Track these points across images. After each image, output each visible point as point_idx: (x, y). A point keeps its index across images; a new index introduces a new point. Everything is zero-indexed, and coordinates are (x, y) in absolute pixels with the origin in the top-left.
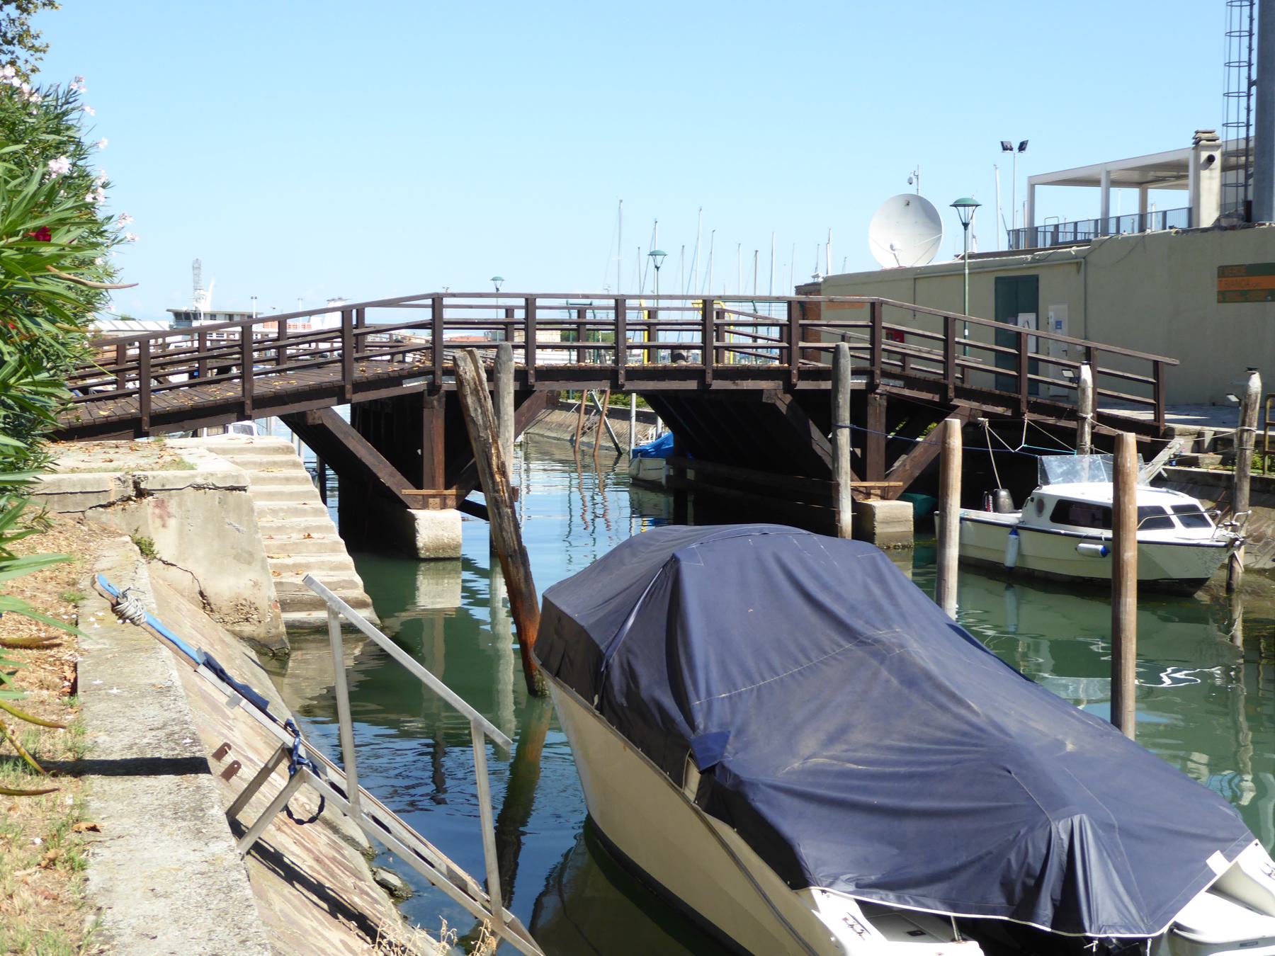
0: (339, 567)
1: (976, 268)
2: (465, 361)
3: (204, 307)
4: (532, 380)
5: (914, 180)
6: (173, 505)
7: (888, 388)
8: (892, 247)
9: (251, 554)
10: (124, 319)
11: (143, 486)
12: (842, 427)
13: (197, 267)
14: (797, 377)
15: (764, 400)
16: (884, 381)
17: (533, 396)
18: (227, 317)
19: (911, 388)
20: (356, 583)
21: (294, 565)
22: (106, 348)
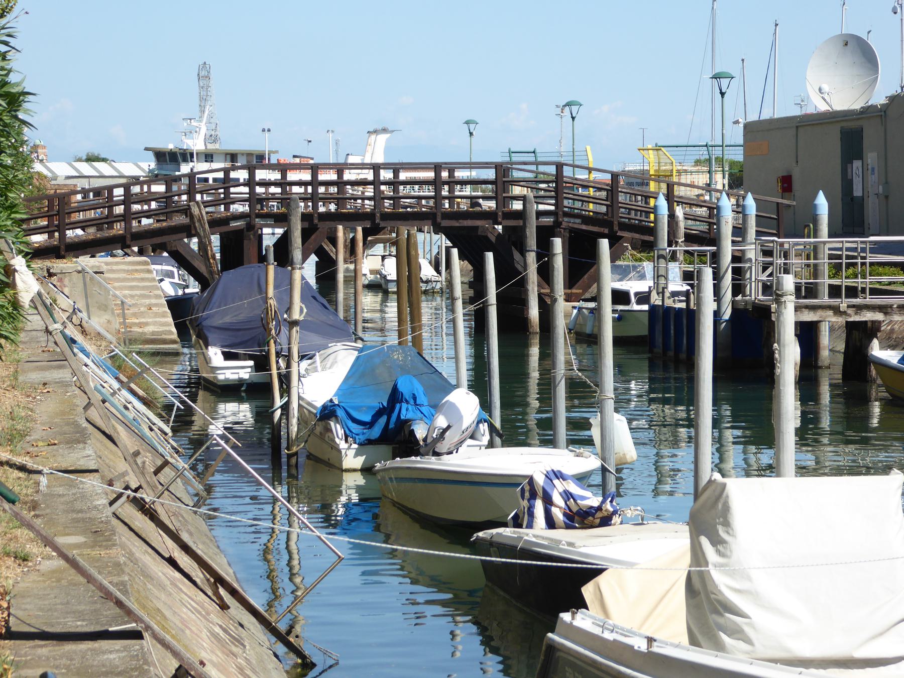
0: (167, 324)
1: (831, 118)
2: (194, 206)
3: (197, 144)
4: (316, 221)
5: (899, 10)
6: (66, 281)
7: (570, 225)
8: (820, 90)
9: (106, 306)
10: (91, 159)
11: (51, 271)
12: (529, 251)
13: (204, 75)
14: (501, 217)
15: (479, 233)
16: (566, 219)
17: (318, 231)
18: (229, 157)
19: (586, 224)
20: (172, 332)
21: (140, 323)
22: (368, 186)
